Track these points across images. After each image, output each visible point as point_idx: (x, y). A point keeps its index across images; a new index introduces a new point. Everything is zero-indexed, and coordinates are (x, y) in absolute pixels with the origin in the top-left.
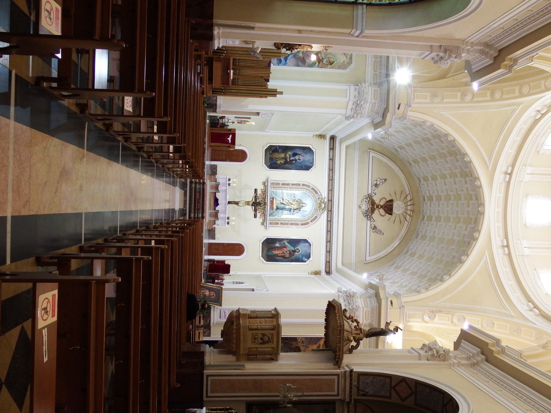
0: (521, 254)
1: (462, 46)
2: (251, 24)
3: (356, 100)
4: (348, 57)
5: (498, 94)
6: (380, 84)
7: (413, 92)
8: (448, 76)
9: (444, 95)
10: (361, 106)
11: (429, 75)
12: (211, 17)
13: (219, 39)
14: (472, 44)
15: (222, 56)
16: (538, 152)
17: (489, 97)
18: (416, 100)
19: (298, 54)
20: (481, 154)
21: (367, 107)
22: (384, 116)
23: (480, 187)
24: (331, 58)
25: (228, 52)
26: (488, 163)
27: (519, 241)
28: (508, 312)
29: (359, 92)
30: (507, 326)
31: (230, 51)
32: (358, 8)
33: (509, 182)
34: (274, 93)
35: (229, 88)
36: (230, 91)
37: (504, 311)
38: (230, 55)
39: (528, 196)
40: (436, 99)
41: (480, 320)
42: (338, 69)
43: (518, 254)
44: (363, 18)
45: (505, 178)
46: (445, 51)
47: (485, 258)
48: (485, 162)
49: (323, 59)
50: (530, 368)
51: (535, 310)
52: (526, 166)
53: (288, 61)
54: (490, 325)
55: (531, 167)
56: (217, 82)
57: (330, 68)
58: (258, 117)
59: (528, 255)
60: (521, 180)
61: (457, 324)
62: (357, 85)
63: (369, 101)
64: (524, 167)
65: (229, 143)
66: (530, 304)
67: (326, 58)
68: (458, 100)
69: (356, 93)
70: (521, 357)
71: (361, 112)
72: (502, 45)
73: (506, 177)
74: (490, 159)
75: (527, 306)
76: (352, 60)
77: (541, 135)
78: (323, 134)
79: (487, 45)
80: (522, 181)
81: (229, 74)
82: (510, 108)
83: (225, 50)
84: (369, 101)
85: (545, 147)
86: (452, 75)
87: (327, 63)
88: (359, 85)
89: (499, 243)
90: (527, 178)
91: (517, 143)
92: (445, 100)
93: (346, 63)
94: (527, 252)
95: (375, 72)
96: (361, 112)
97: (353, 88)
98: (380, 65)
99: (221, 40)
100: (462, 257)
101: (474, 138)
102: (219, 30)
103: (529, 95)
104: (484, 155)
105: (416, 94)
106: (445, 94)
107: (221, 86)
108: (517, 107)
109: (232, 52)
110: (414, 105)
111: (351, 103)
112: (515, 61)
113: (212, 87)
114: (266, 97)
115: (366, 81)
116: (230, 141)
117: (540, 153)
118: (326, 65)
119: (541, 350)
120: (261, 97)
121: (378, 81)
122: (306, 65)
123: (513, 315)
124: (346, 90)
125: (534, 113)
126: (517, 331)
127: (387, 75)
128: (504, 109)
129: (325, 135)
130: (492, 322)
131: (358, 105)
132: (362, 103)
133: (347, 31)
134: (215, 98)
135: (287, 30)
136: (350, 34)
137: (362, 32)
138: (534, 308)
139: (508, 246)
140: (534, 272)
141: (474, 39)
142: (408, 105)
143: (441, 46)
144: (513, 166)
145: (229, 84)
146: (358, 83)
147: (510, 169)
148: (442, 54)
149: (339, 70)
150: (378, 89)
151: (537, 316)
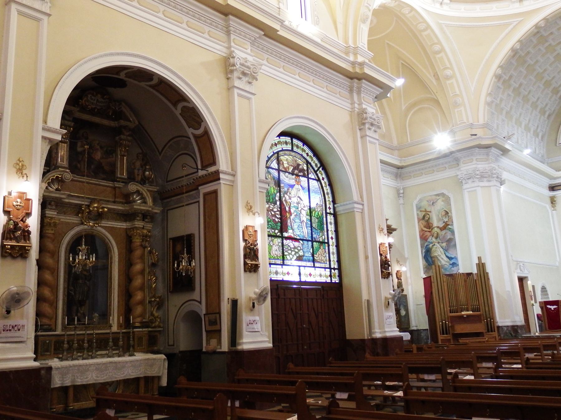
1: (356, 112)
2: (364, 305)
3: (477, 180)
4: (438, 198)
5: (435, 48)
6: (457, 160)
7: (458, 126)
8: (436, 98)
9: (453, 95)
10: (482, 172)
11: (439, 116)
12: (363, 341)
13: (385, 332)
14: (353, 103)
15: (449, 325)
17: (442, 54)
18: (465, 120)
19: (444, 248)
20: (507, 34)
21: (482, 166)
22: (488, 147)
24: (441, 215)
25: (443, 319)
26: (515, 23)
29: (468, 179)
31: (443, 317)
32: (339, 211)
34: (481, 266)
35: (484, 314)
36: (487, 313)
38: (446, 316)
40: (458, 102)
42: (450, 205)
44: (344, 205)
46: (364, 124)
48: (514, 27)
49: (444, 222)
53: (453, 256)
56: (479, 327)
57: (451, 213)
58: (529, 278)
62: (462, 182)
63: (474, 166)
65: (558, 308)
67: (443, 219)
68: (453, 81)
69: (470, 181)
71: (489, 171)
72: (344, 79)
74: (510, 24)
76: (439, 194)
78: (549, 201)
79: (351, 91)
81: (468, 316)
83: (442, 322)
84: (474, 166)
86: (434, 95)
87: (447, 217)
88: (460, 180)
92: (458, 93)
93: (444, 199)
95: (447, 168)
96: (489, 171)
97: (465, 186)
98: (439, 165)
99: (386, 330)
102: (376, 332)
103: (425, 21)
104: (507, 31)
105: (459, 123)
106: (451, 95)
107: (483, 322)
109: (443, 314)
110: (471, 121)
111: (482, 184)
112: (353, 64)
113: (486, 332)
114: (487, 273)
115: (455, 174)
116: (555, 307)
118: (449, 217)
120: (488, 279)
121: (455, 163)
122: (453, 237)
124: (469, 192)
127: (445, 156)
129: (550, 197)
131: (483, 176)
132: (478, 172)
133: (358, 217)
134: (505, 328)
135: (367, 270)
136: (362, 212)
137: (355, 203)
141: (347, 105)
142: (471, 126)
143: (360, 130)
145: (480, 315)
146: (459, 183)
148: (367, 126)
149: (451, 203)
150: (462, 161)
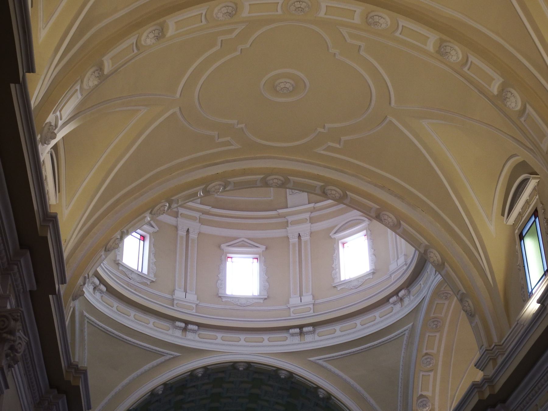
0: (311, 306)
16: (153, 282)
23: (205, 368)
26: (168, 357)
27: (292, 310)
28: (407, 332)
30: (429, 336)
33: (199, 325)
37: (405, 338)
39: (220, 295)
41: (421, 374)
43: (312, 311)
45: (193, 330)
47: (320, 362)
50: (512, 355)
51: (400, 294)
52: (173, 299)
54: (429, 360)
55: (176, 291)
59: (313, 296)
60: (194, 306)
61: (430, 407)
64: (175, 302)
66: (391, 300)
70: (491, 350)
73: (191, 330)
74: (162, 354)
75: (395, 305)
77: (128, 280)
80: (197, 305)
82: (86, 330)
85: (145, 271)
89: (297, 339)
90: (192, 297)
91: (141, 315)
94: (307, 299)
100: (321, 396)
101: (126, 381)
108: (87, 320)
117: (154, 280)
119: (477, 319)
123: (410, 325)
125: (98, 295)
126: (435, 323)
128: (86, 338)
130: (423, 357)
138: (398, 295)
139: (301, 327)
140: (339, 288)
144: (173, 319)
147: (178, 324)
151: (409, 292)
